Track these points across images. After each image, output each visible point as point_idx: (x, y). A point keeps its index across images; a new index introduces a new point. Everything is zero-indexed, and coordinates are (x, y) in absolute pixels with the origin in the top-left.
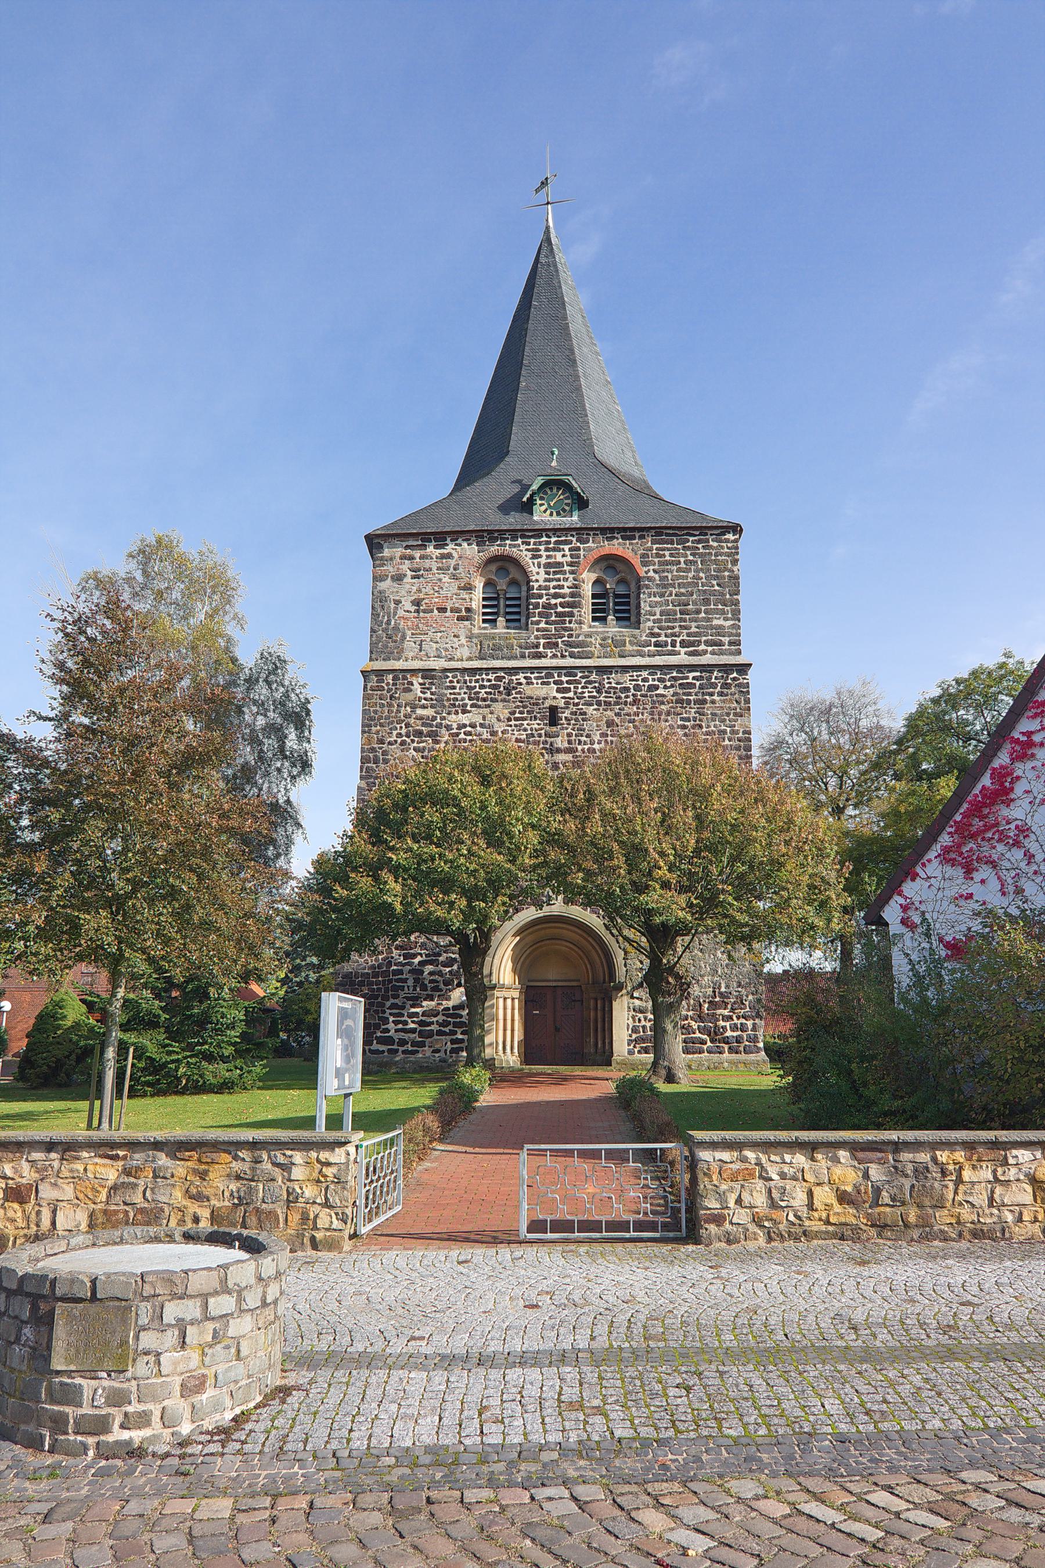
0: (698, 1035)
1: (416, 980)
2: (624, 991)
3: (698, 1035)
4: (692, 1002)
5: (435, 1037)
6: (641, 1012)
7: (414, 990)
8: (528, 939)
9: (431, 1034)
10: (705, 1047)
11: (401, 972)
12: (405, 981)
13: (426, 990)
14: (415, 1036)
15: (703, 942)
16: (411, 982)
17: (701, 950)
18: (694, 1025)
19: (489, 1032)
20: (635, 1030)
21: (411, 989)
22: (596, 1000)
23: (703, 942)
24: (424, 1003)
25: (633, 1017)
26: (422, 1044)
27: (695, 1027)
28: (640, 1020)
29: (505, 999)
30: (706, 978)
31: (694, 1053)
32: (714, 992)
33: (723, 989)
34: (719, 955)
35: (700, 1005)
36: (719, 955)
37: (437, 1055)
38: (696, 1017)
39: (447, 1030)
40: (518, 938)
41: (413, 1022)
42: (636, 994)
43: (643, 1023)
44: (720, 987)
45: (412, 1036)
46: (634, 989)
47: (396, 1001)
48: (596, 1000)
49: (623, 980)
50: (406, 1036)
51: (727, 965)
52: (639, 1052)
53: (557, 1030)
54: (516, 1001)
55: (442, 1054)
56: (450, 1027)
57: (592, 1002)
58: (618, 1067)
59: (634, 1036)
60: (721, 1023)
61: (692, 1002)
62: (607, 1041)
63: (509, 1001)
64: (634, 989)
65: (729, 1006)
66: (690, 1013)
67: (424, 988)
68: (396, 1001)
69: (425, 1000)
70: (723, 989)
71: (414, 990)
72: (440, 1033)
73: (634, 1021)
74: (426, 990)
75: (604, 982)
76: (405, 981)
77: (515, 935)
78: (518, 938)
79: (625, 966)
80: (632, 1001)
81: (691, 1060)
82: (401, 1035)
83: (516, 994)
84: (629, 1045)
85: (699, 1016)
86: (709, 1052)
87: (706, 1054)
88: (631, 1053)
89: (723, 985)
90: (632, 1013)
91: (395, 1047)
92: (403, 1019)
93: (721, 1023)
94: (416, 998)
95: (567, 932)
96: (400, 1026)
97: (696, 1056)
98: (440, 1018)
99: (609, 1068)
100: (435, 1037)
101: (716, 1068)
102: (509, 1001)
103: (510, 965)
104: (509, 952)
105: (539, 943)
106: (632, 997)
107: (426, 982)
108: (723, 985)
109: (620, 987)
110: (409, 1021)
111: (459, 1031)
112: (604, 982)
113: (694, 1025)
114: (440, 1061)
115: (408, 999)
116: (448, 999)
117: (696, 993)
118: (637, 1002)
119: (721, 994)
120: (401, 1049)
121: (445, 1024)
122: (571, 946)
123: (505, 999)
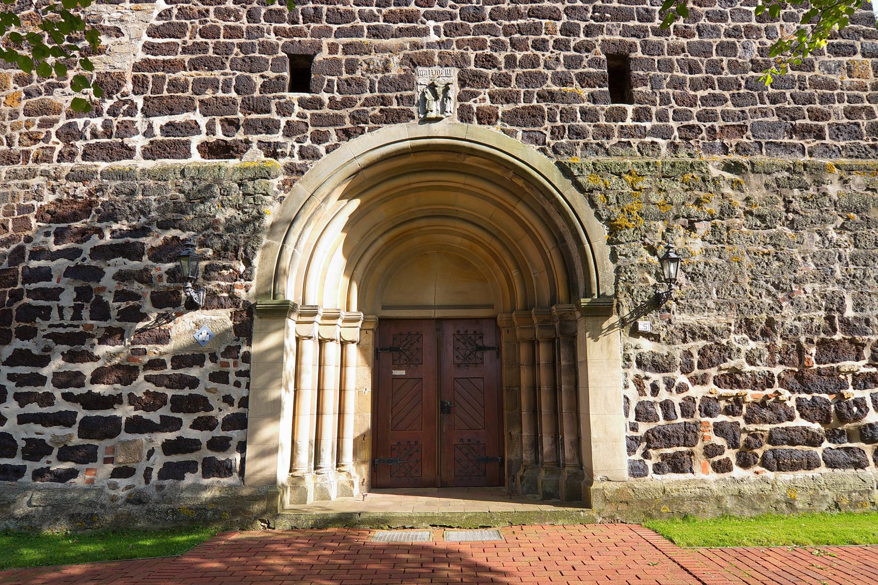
0: (799, 422)
1: (83, 294)
2: (614, 319)
3: (799, 422)
4: (779, 342)
5: (124, 436)
6: (658, 367)
7: (77, 316)
8: (382, 213)
9: (110, 428)
10: (819, 451)
11: (46, 274)
12: (54, 294)
13: (106, 317)
14: (73, 436)
15: (795, 205)
16: (68, 299)
17: (792, 224)
18: (790, 398)
19: (274, 410)
20: (643, 413)
21: (68, 314)
22: (533, 344)
23: (795, 205)
24: (101, 350)
25: (639, 383)
26: (88, 456)
27: (792, 404)
28: (655, 389)
29: (322, 342)
30: (808, 287)
31: (794, 467)
32: (830, 319)
33: (849, 313)
34: (833, 234)
35: (800, 351)
36: (833, 234)
37: (123, 482)
38: (791, 379)
39: (154, 417)
40: (356, 203)
41: (67, 397)
42: (644, 325)
43: (664, 395)
44: (841, 309)
45: (58, 431)
46: (639, 311)
47: (28, 345)
48: (533, 344)
49: (610, 292)
50: (49, 433)
51: (854, 259)
52: (658, 469)
53: (445, 409)
54: (352, 349)
55: (137, 481)
56: (165, 411)
57: (524, 352)
58: (609, 509)
59: (643, 428)
60: (852, 394)
61: (779, 342)
62: (567, 439)
63: (332, 351)
64: (639, 311)
65: (867, 353)
66: (778, 370)
67: (101, 311)
68: (28, 345)
69: (102, 341)
70: (849, 313)
71: (77, 316)
72: (137, 426)
73: (642, 392)
74: (106, 317)
75: (554, 301)
76: (54, 294)
77: (347, 195)
78: (356, 203)
79: (614, 257)
80: (634, 341)
81: (793, 487)
82: (34, 430)
83: (353, 333)
84: (631, 450)
85: (799, 377)
86: (832, 464)
87: (823, 469)
88: (637, 471)
89: (849, 303)
90: (634, 371)
91: (16, 461)
92: (41, 390)
93: (852, 394)
94: (81, 338)
95: (469, 198)
96: (34, 408)
97: (801, 474)
98: (141, 386)
99: (584, 513)
100: (124, 436)
101: (854, 504)
102: (332, 351)
103: (340, 261)
104: (336, 237)
105: (411, 210)
106: (635, 332)
107: (108, 298)
108: (849, 303)
109: (603, 309)
110: (58, 393)
111: (187, 419)
112: (554, 301)
113: (790, 398)
114: (129, 501)
115: (59, 339)
116: (163, 339)
117: (789, 322)
118: (647, 346)
119: (845, 322)
120: (32, 466)
121: (154, 401)
122: (497, 246)
123: (322, 342)
